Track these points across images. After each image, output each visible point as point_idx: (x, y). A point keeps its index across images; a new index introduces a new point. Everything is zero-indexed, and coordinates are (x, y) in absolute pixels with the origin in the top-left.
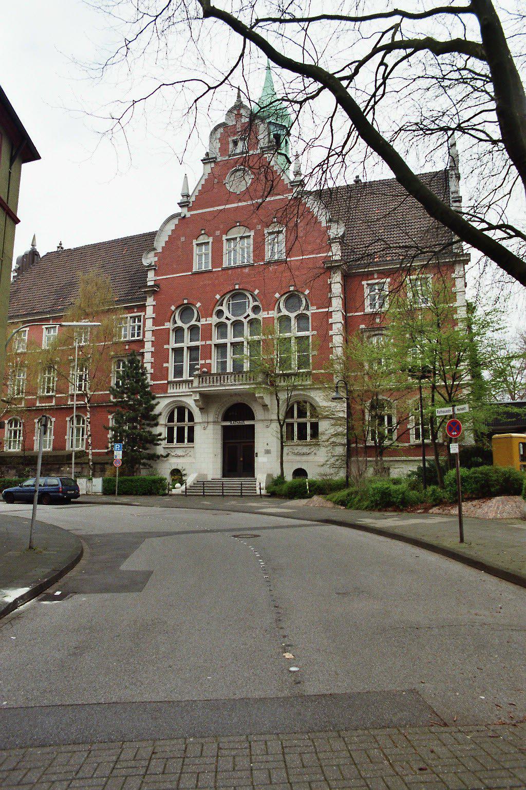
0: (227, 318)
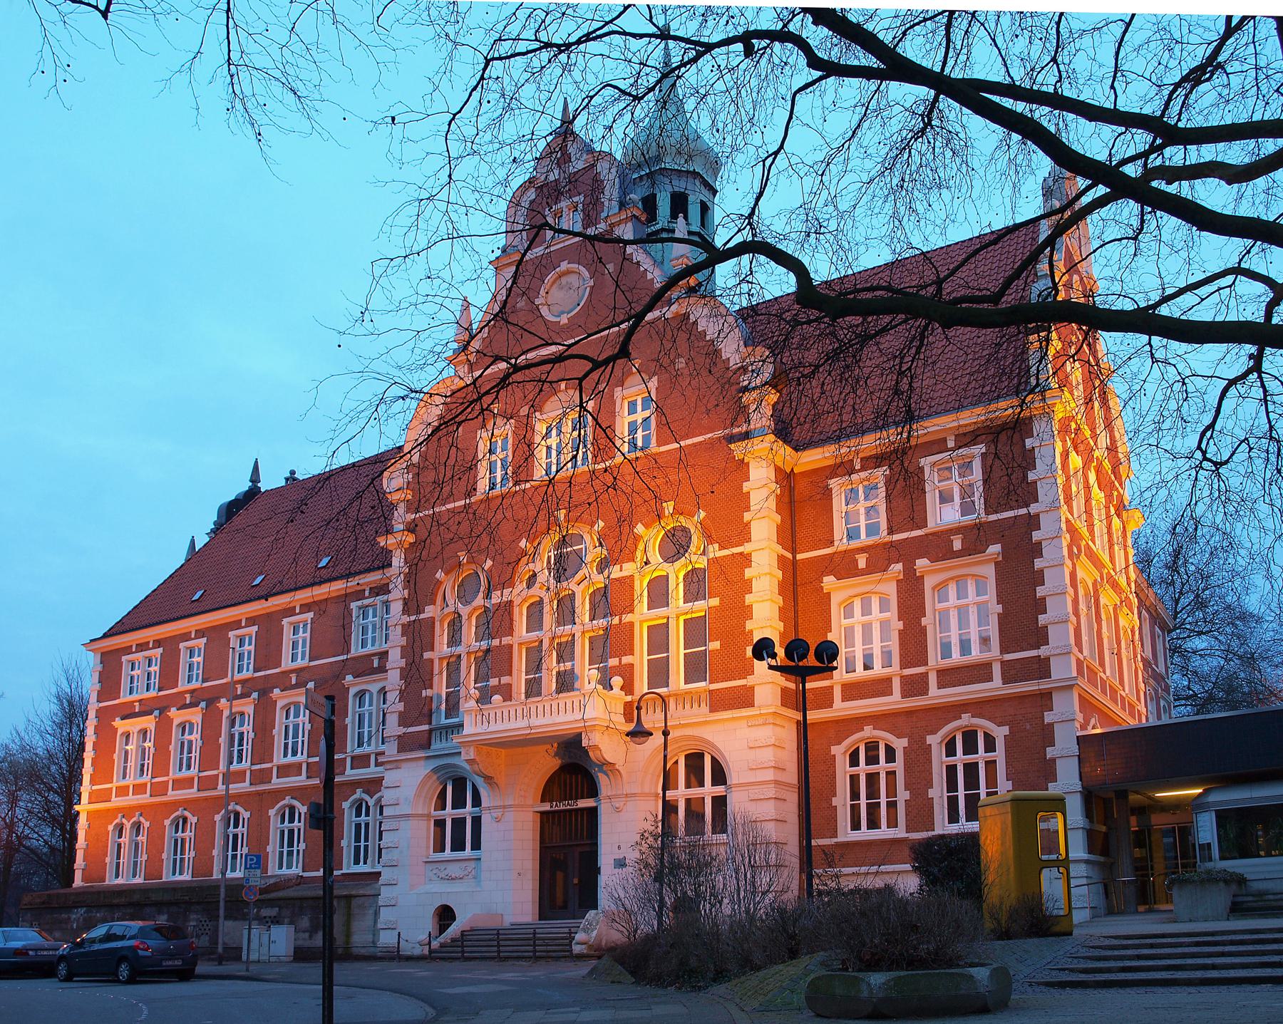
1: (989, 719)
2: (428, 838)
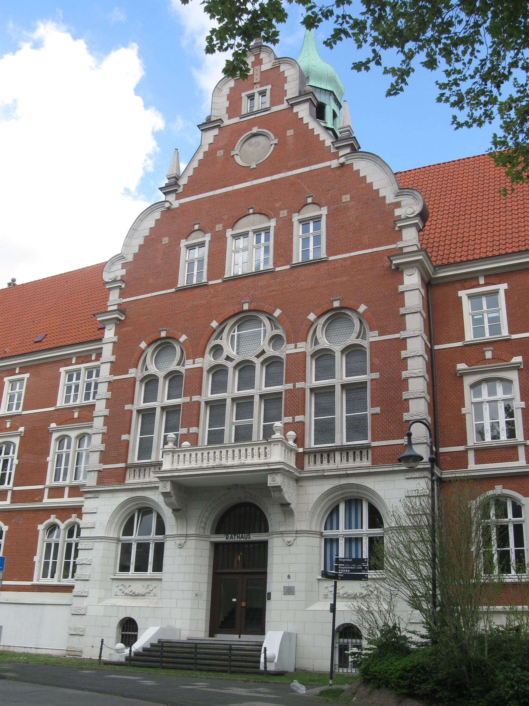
0: (228, 358)
1: (516, 491)
2: (116, 558)
